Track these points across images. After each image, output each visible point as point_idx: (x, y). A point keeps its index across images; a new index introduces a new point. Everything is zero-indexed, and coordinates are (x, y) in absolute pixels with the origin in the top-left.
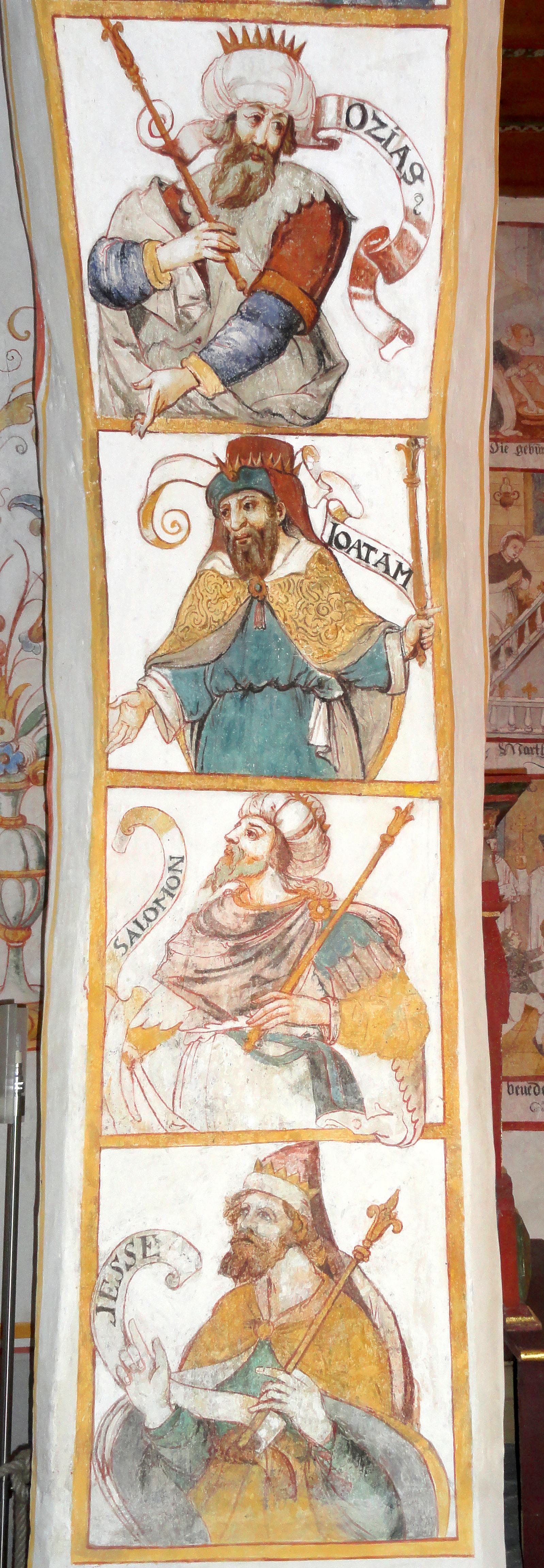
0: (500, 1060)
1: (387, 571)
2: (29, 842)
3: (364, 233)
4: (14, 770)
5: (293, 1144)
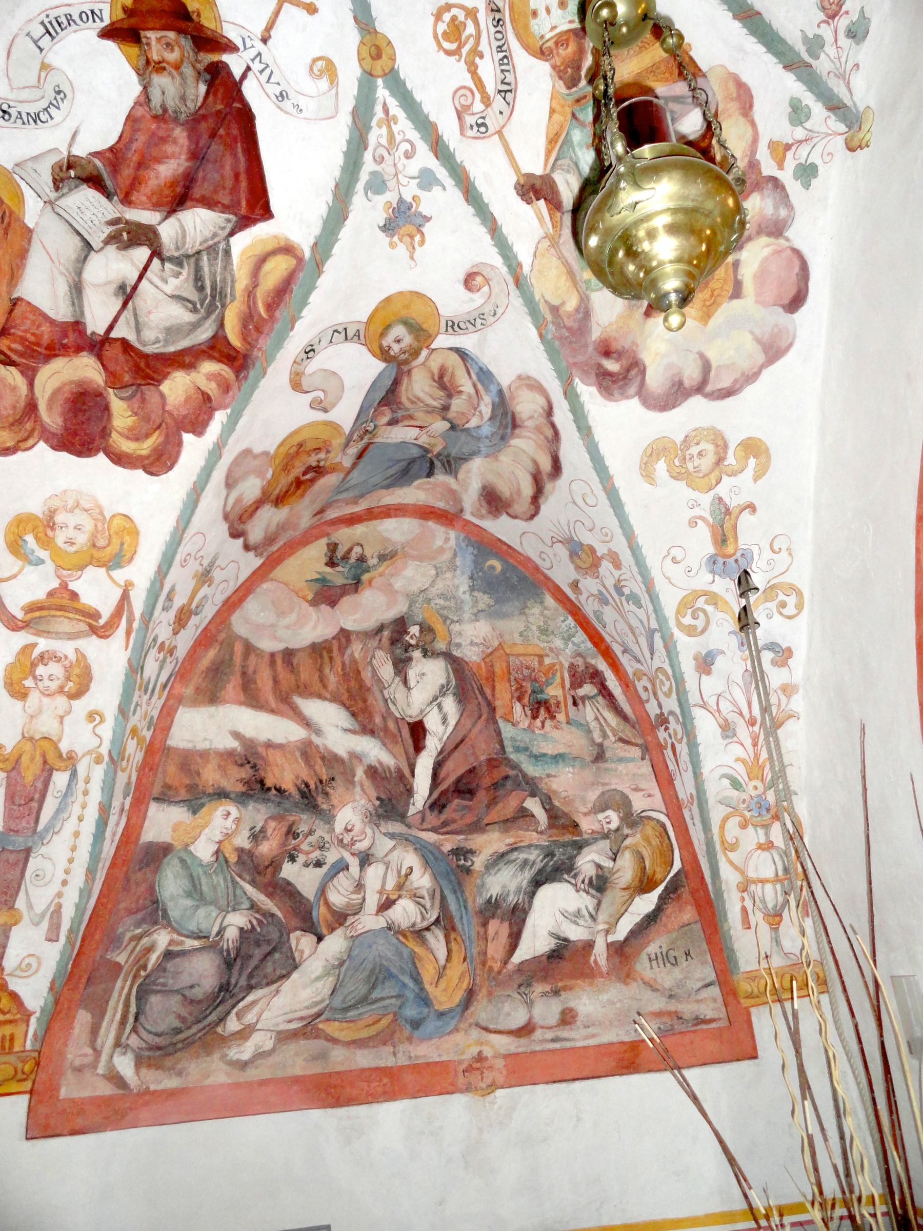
0: (671, 782)
1: (505, 57)
2: (777, 858)
3: (255, 110)
4: (764, 812)
5: (384, 1022)
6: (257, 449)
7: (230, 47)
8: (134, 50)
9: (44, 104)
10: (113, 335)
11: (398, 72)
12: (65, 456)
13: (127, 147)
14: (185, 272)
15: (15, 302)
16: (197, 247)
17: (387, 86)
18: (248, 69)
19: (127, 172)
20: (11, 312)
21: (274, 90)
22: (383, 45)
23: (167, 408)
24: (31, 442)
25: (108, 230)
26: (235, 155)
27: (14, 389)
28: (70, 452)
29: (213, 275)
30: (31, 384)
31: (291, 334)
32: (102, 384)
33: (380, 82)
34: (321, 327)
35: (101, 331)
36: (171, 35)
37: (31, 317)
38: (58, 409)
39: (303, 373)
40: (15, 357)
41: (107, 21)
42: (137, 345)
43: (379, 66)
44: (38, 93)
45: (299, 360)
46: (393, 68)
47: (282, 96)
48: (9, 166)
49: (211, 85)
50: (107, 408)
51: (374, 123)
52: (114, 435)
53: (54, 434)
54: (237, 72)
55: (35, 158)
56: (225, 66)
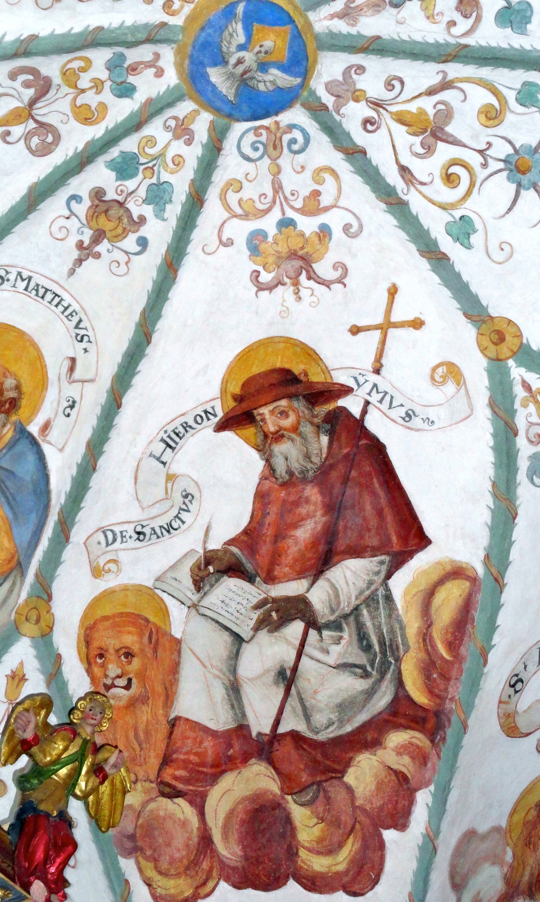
3: (383, 439)
6: (483, 828)
7: (346, 391)
8: (250, 431)
9: (174, 512)
10: (281, 730)
11: (528, 346)
12: (250, 892)
13: (261, 524)
14: (346, 635)
15: (174, 723)
16: (354, 602)
17: (520, 364)
18: (367, 403)
19: (265, 549)
20: (171, 733)
21: (398, 413)
22: (503, 327)
23: (358, 803)
24: (210, 885)
25: (255, 615)
26: (373, 493)
27: (184, 824)
28: (256, 887)
29: (378, 628)
30: (202, 814)
31: (486, 670)
32: (278, 792)
33: (511, 363)
34: (523, 649)
35: (267, 730)
36: (284, 403)
37: (192, 734)
38: (234, 837)
39: (516, 712)
40: (180, 786)
41: (220, 414)
42: (309, 734)
43: (504, 350)
44: (168, 503)
45: (505, 698)
46: (522, 343)
47: (409, 416)
48: (149, 584)
49: (332, 434)
50: (288, 820)
51: (517, 405)
52: (303, 853)
53: (234, 869)
54: (356, 412)
55: (173, 567)
56: (343, 410)
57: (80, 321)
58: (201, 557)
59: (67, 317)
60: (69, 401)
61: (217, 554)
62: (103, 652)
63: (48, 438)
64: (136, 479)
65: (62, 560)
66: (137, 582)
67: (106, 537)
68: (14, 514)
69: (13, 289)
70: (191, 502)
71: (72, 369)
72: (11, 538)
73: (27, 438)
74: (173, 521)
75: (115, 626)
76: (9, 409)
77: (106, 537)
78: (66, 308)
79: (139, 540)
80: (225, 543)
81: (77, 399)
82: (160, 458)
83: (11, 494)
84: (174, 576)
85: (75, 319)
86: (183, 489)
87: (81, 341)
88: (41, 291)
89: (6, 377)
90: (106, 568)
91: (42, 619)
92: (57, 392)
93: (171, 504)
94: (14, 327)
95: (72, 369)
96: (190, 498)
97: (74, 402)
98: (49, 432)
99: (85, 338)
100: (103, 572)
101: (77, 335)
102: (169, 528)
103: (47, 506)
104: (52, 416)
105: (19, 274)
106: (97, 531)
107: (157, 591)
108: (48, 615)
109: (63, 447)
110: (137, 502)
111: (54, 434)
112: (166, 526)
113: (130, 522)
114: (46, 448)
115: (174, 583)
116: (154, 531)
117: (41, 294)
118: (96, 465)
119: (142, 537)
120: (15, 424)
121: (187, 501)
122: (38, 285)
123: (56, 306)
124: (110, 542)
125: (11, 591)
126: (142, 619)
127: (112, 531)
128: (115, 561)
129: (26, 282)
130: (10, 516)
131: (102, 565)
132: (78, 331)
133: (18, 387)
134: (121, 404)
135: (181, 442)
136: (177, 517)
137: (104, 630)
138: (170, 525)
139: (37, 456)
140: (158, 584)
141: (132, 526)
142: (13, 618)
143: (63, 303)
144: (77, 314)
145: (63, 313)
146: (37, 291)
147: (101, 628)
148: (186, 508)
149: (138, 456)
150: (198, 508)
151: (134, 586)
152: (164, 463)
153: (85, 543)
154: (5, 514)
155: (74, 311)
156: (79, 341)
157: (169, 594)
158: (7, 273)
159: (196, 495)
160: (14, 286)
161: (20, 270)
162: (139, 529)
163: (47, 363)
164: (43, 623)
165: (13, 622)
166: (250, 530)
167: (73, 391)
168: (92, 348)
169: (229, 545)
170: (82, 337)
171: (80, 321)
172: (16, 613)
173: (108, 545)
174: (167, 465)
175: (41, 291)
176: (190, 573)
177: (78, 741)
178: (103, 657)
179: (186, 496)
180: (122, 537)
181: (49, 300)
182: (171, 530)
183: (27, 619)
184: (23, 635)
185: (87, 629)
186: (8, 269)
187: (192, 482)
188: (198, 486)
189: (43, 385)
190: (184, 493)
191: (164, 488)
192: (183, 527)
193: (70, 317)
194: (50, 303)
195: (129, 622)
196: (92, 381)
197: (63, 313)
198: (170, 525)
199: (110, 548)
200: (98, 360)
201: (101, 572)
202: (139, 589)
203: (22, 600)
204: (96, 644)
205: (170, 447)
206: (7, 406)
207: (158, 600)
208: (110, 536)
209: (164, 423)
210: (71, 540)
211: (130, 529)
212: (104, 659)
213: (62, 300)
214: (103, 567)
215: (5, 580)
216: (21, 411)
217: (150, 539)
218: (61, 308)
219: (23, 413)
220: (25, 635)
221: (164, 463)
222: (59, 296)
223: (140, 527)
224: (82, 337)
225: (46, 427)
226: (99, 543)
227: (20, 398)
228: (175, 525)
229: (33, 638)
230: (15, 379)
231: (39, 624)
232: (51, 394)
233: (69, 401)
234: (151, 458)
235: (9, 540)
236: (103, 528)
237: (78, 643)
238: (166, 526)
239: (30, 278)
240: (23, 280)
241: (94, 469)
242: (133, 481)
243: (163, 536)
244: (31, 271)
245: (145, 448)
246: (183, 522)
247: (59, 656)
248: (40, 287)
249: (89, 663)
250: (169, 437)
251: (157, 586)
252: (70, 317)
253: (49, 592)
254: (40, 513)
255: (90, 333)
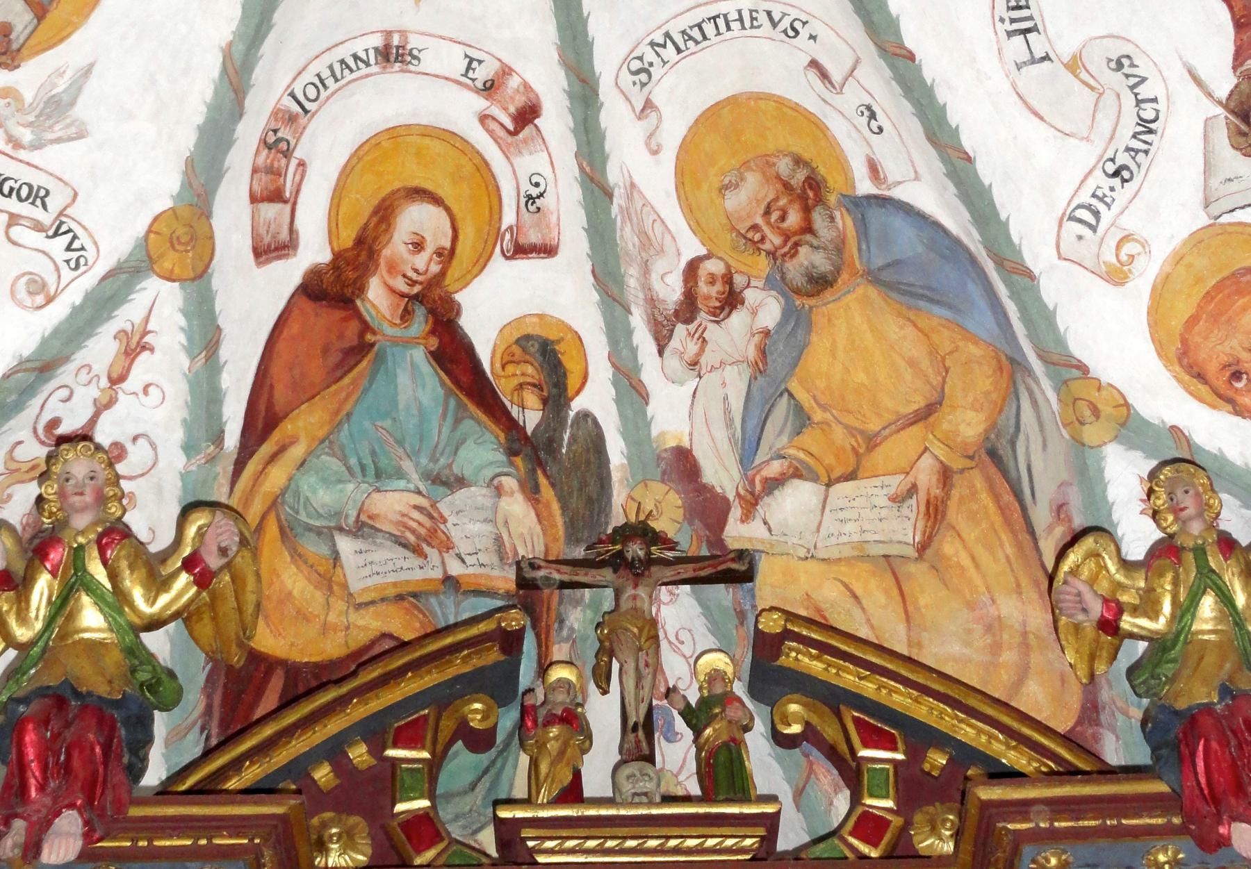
9: (1128, 100)
44: (1109, 98)
48: (1204, 221)
57: (769, 13)
58: (1226, 118)
59: (752, 27)
60: (862, 113)
61: (1241, 92)
62: (1234, 368)
63: (891, 179)
64: (1036, 114)
65: (1051, 307)
66: (1185, 234)
67: (1080, 221)
68: (950, 307)
69: (668, 66)
70: (1132, 65)
71: (824, 75)
72: (976, 340)
73: (869, 205)
74: (1141, 112)
75: (1215, 319)
76: (816, 195)
77: (1080, 221)
78: (741, 20)
79: (1127, 181)
80: (1235, 68)
81: (868, 100)
82: (1033, 57)
83: (922, 287)
84: (1222, 178)
85: (762, 18)
86: (1105, 61)
87: (797, 33)
88: (696, 33)
89: (774, 165)
90: (1124, 258)
91: (1100, 406)
92: (841, 118)
93: (1113, 96)
94: (718, 103)
95: (824, 75)
96: (1125, 62)
97: (869, 108)
98: (884, 172)
99: (798, 25)
100: (1125, 268)
101: (785, 32)
102: (1147, 127)
103: (973, 260)
104: (868, 151)
105: (653, 44)
106: (1060, 225)
107: (1225, 219)
108: (1104, 393)
109: (916, 172)
110: (1071, 140)
111: (893, 168)
112: (1141, 129)
113: (1090, 172)
114: (898, 193)
115: (1233, 187)
116: (1132, 150)
117: (699, 38)
118: (967, 153)
119: (1126, 174)
120: (840, 204)
121: (1126, 70)
122: (684, 32)
123: (729, 28)
124: (1093, 222)
125: (1034, 403)
126: (1244, 275)
127: (1079, 207)
128: (1126, 238)
129: (669, 43)
130: (947, 313)
131: (1114, 261)
132: (781, 27)
133: (798, 161)
134: (911, 52)
135: (1033, 11)
136: (1139, 102)
137: (1206, 338)
138: (1142, 121)
139: (901, 214)
140: (1215, 209)
141: (1098, 173)
142: (1067, 436)
143: (730, 18)
144: (757, 11)
145: (743, 28)
146: (691, 38)
147: (1198, 339)
148: (1137, 80)
149: (1007, 86)
150: (1151, 63)
151: (1185, 243)
152: (1046, 58)
153: (1060, 257)
154: (940, 317)
155: (751, 11)
156: (794, 37)
157: (1242, 208)
158: (640, 58)
159: (1127, 49)
160: (665, 63)
161: (648, 40)
162: (1111, 168)
163: (795, 100)
164: (1106, 410)
165: (1073, 442)
166: (1242, 17)
167: (852, 99)
168: (816, 27)
169: (1241, 65)
170: (793, 29)
171: (769, 13)
172: (1065, 426)
173: (1094, 229)
174: (1052, 55)
175: (696, 33)
176: (1238, 153)
177: (1189, 557)
178: (1241, 373)
179: (1120, 65)
180: (1101, 200)
181: (715, 32)
182: (1152, 126)
183: (1082, 423)
184: (1100, 446)
185: (1180, 361)
186: (637, 53)
187: (1105, 41)
188: (1117, 37)
189: (818, 127)
190: (1113, 65)
191: (1083, 87)
192: (1162, 106)
193: (755, 23)
194: (719, 34)
195: (1229, 296)
196: (857, 61)
197: (743, 28)
198: (1142, 121)
199: (1101, 228)
200: (837, 33)
201: (1122, 271)
202: (1197, 241)
203: (1055, 405)
204: (1212, 369)
205: (1028, 31)
206: (811, 194)
207: (1240, 229)
208: (1085, 215)
209: (989, 13)
210: (1036, 272)
211: (1100, 181)
212: (1245, 376)
213: (725, 16)
214: (1119, 261)
215: (1018, 400)
216: (831, 183)
217: (1139, 166)
218: (735, 26)
219: (834, 181)
220: (1105, 443)
221: (1046, 58)
222: (718, 16)
223: (1109, 164)
224: (793, 29)
225: (874, 170)
226: (1080, 238)
227: (813, 170)
228: (1148, 114)
229: (1116, 437)
230: (786, 155)
231: (1103, 414)
232: (839, 128)
233: (862, 113)
234: (1024, 70)
235: (976, 343)
236: (1064, 214)
237: (1187, 389)
238: (1141, 129)
239: (667, 35)
240: (664, 46)
241: (969, 159)
242: (1036, 120)
243: (1150, 144)
244: (659, 28)
245: (1003, 67)
246: (1155, 100)
247: (1174, 429)
248: (688, 31)
249: (1230, 401)
250: (1013, 21)
251: (1217, 214)
252: (755, 23)
253: (1075, 362)
254: (973, 275)
255: (795, 13)
